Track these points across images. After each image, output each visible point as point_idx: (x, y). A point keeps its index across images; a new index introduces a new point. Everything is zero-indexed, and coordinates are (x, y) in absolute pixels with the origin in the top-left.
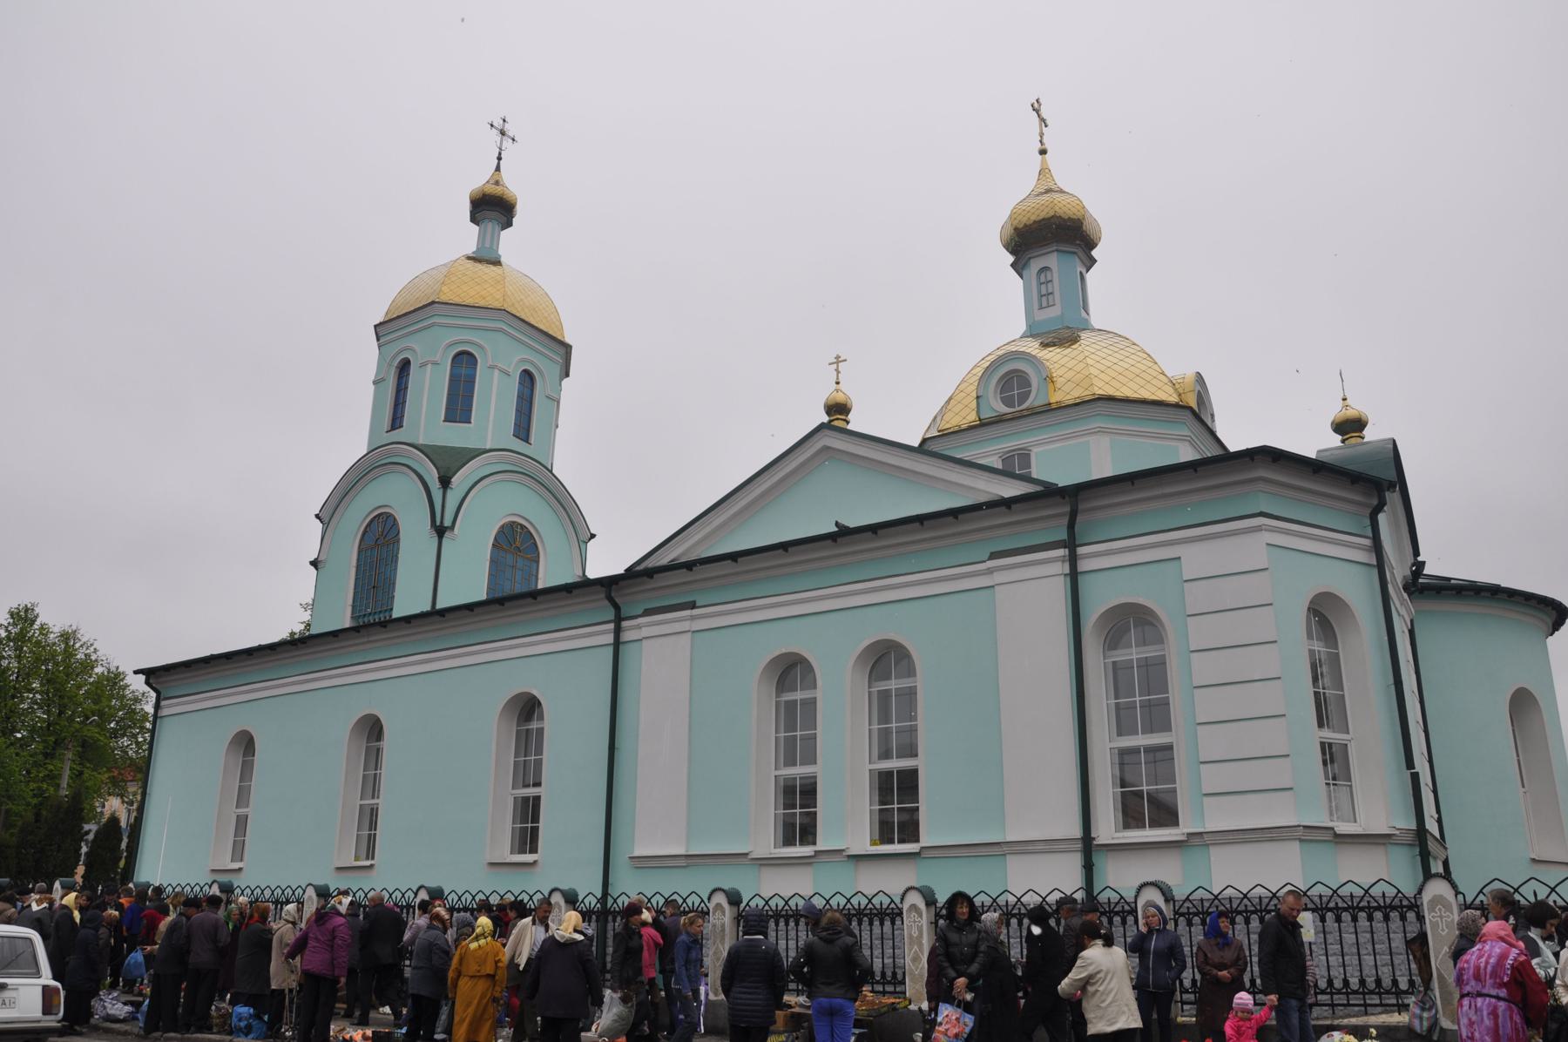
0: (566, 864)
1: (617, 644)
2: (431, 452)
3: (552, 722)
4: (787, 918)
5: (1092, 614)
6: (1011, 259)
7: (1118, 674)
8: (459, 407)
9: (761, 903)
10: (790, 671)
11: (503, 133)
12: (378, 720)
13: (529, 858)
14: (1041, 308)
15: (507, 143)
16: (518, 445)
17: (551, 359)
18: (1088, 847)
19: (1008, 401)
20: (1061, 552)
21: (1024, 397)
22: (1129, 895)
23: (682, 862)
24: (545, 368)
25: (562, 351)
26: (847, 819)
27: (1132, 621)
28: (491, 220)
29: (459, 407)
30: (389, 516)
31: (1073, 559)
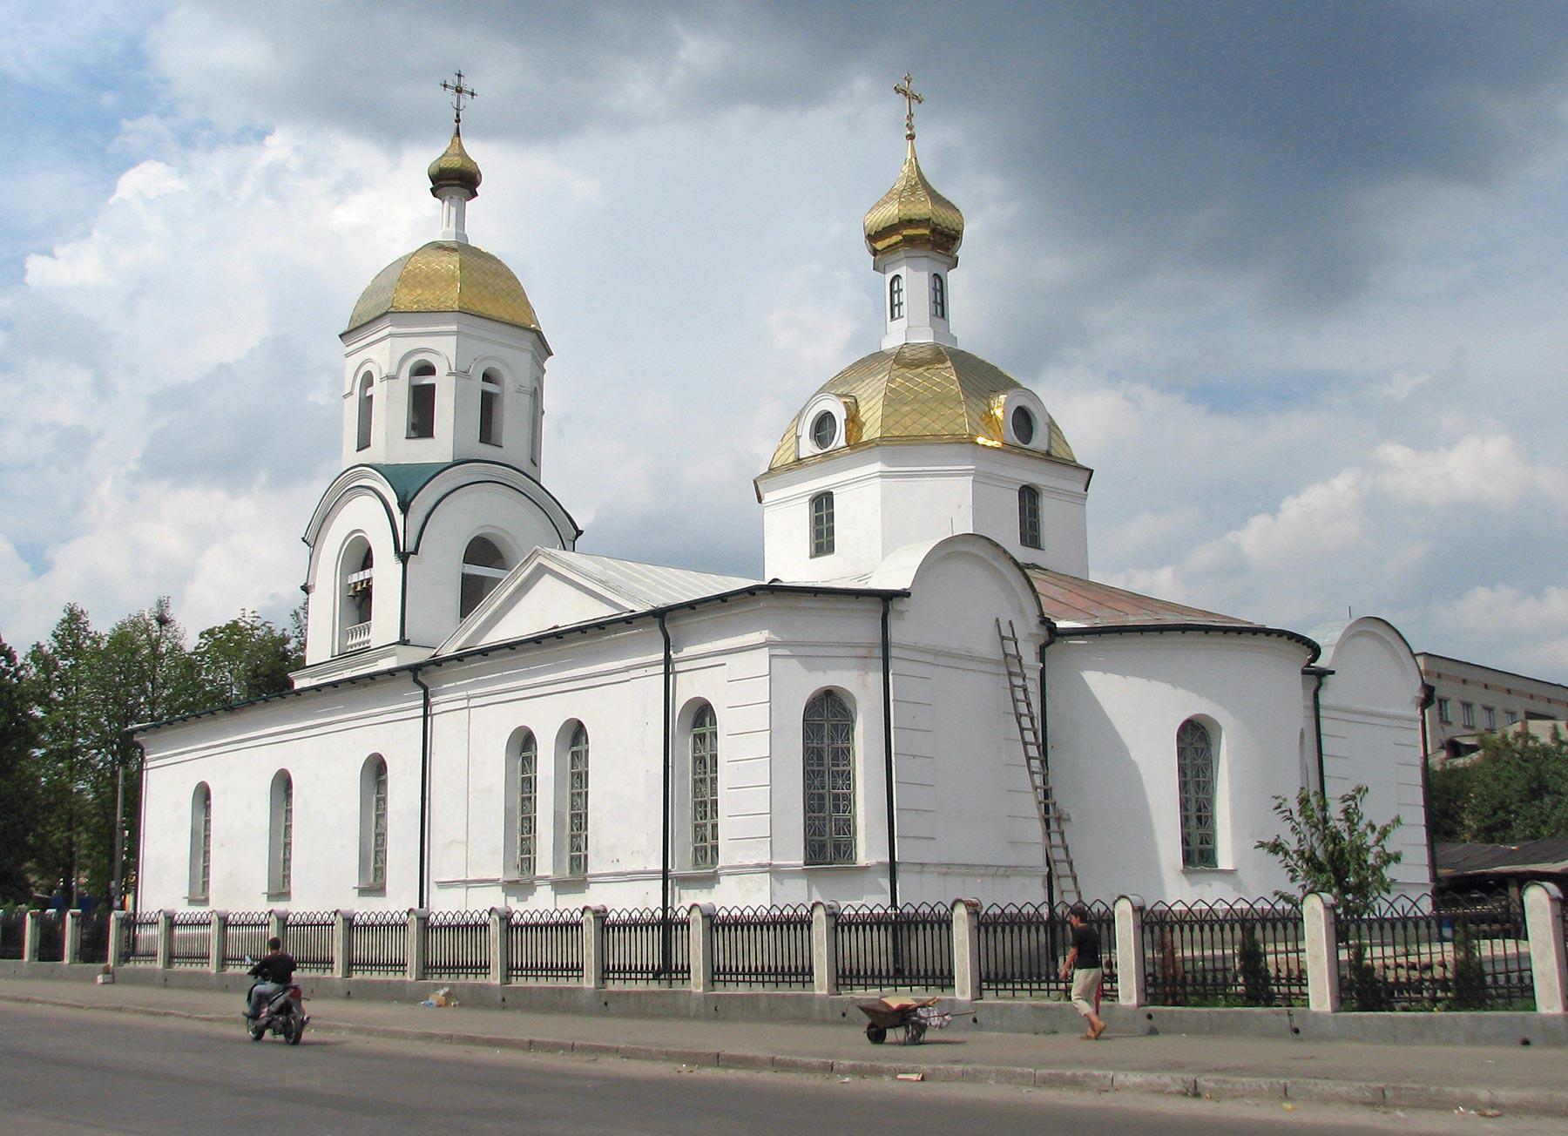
0: (398, 900)
1: (668, 661)
2: (391, 473)
3: (725, 721)
4: (879, 924)
6: (102, 624)
8: (421, 424)
9: (1032, 911)
10: (524, 742)
11: (459, 90)
12: (384, 763)
15: (466, 100)
17: (519, 349)
23: (964, 870)
24: (512, 360)
29: (421, 424)
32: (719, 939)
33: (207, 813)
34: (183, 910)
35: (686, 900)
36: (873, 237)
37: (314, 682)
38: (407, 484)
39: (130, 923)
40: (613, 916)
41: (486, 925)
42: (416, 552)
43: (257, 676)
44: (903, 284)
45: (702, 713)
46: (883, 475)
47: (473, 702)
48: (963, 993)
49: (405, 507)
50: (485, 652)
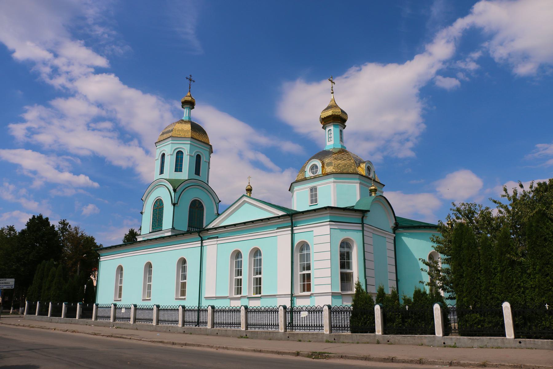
0: (191, 302)
1: (202, 246)
2: (171, 181)
3: (188, 265)
4: (339, 312)
5: (296, 243)
7: (302, 256)
8: (178, 168)
10: (237, 255)
11: (191, 80)
13: (183, 297)
14: (329, 141)
16: (197, 177)
18: (292, 296)
19: (313, 173)
20: (290, 229)
21: (316, 172)
22: (322, 306)
25: (209, 147)
26: (247, 289)
27: (304, 246)
28: (187, 108)
30: (161, 199)
31: (292, 230)
32: (249, 315)
33: (121, 276)
34: (140, 304)
35: (299, 303)
36: (175, 171)
37: (144, 239)
38: (176, 185)
40: (187, 308)
41: (178, 310)
42: (177, 204)
44: (332, 132)
45: (304, 246)
46: (334, 182)
47: (219, 242)
48: (281, 330)
49: (175, 190)
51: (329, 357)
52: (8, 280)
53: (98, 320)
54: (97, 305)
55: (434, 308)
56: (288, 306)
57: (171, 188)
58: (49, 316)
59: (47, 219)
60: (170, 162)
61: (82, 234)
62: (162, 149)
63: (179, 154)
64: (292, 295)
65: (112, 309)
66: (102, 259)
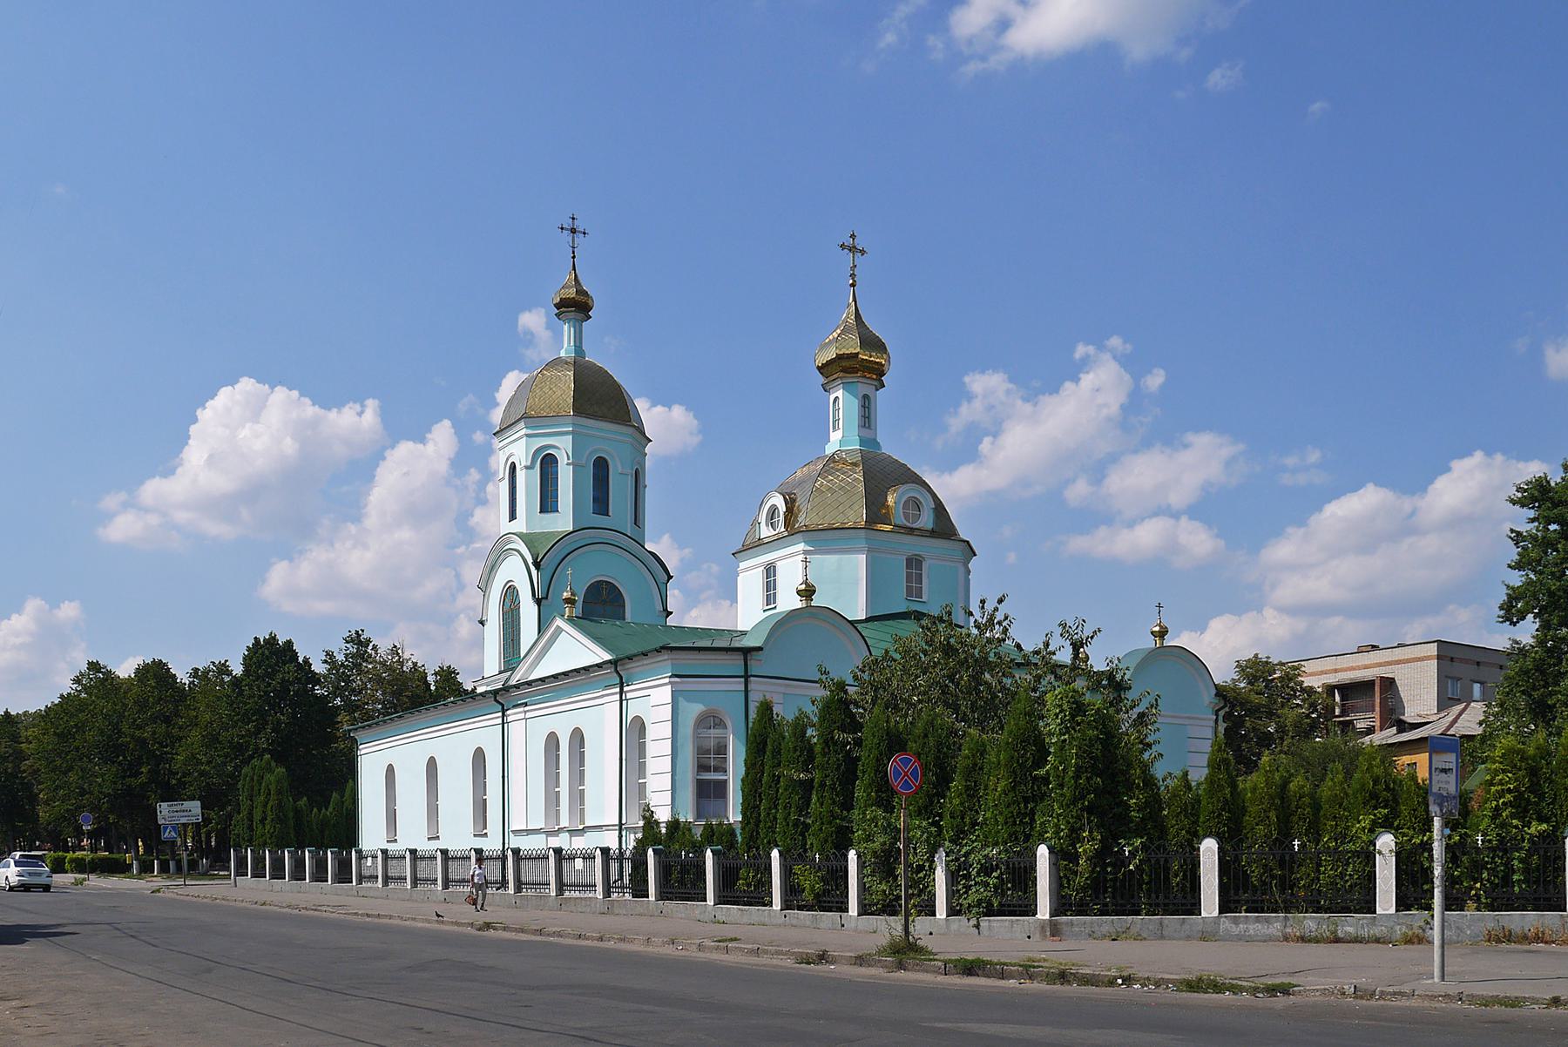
2: (528, 539)
8: (548, 503)
11: (573, 231)
15: (579, 238)
16: (600, 520)
34: (425, 846)
39: (361, 856)
43: (420, 695)
47: (529, 715)
50: (529, 683)
51: (1003, 976)
52: (187, 804)
53: (391, 886)
54: (359, 852)
55: (1202, 848)
56: (614, 845)
57: (530, 561)
58: (652, 898)
59: (289, 643)
60: (528, 483)
61: (415, 664)
62: (508, 451)
63: (548, 464)
64: (621, 824)
65: (598, 860)
66: (363, 749)
